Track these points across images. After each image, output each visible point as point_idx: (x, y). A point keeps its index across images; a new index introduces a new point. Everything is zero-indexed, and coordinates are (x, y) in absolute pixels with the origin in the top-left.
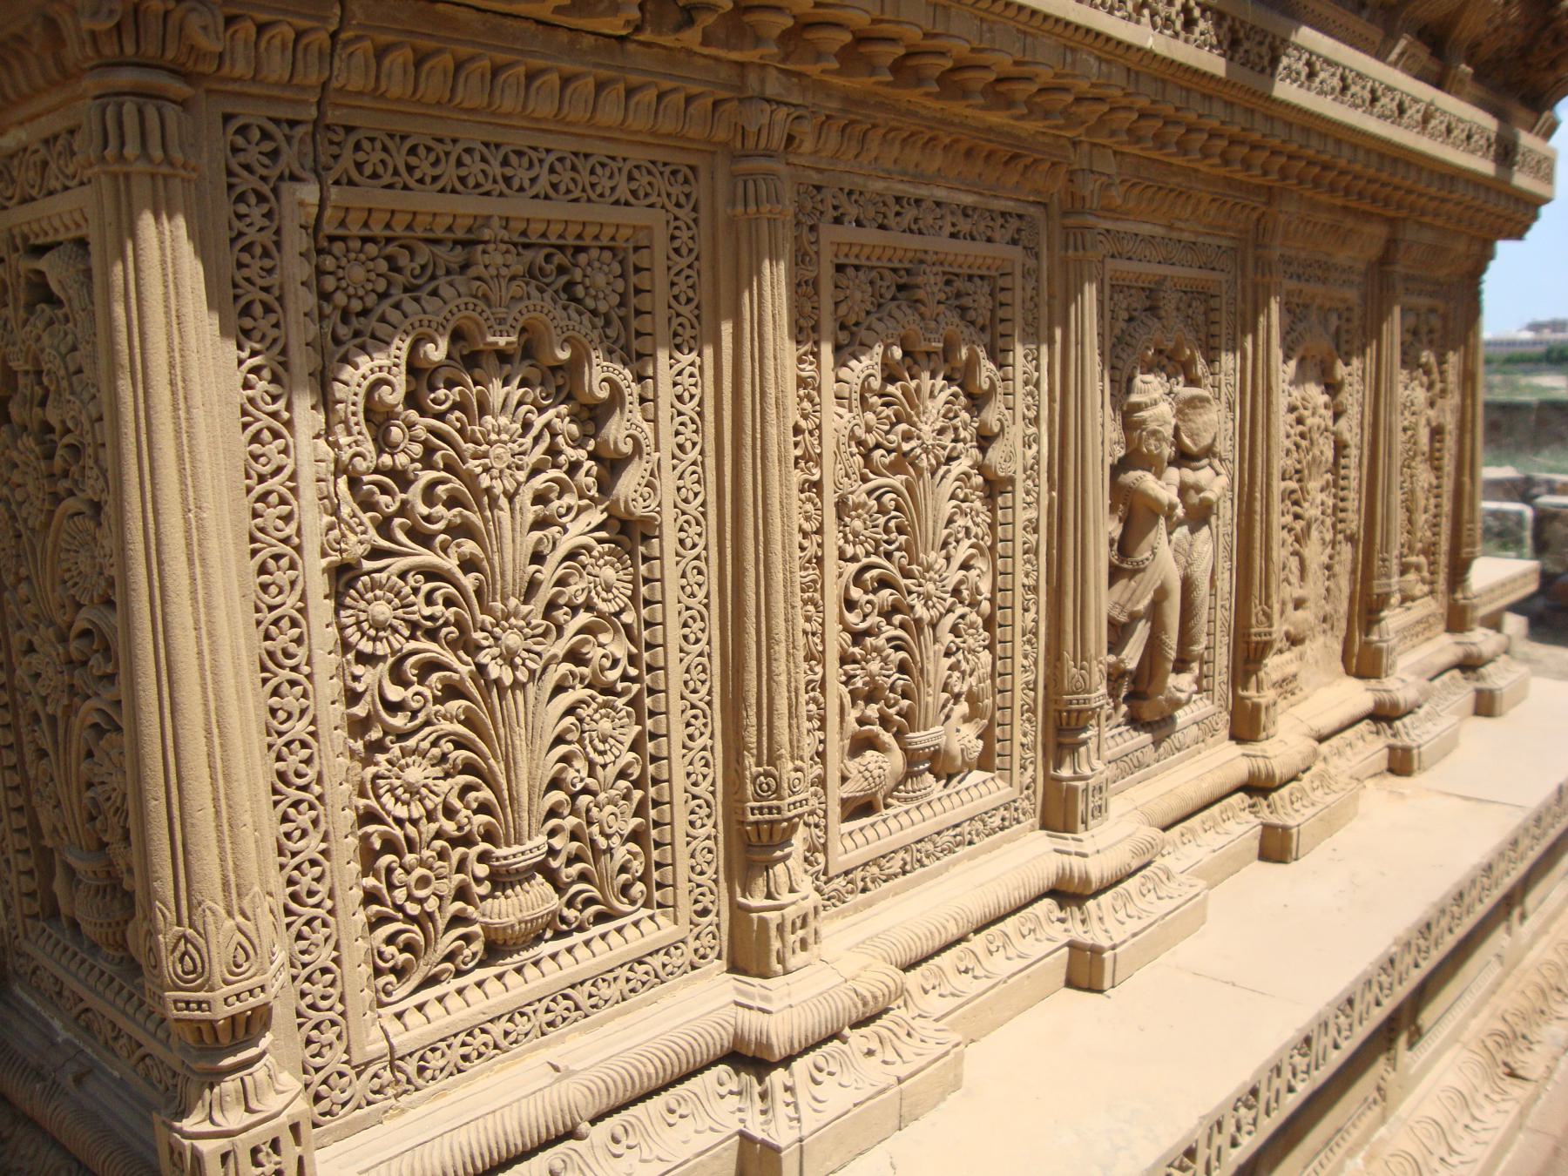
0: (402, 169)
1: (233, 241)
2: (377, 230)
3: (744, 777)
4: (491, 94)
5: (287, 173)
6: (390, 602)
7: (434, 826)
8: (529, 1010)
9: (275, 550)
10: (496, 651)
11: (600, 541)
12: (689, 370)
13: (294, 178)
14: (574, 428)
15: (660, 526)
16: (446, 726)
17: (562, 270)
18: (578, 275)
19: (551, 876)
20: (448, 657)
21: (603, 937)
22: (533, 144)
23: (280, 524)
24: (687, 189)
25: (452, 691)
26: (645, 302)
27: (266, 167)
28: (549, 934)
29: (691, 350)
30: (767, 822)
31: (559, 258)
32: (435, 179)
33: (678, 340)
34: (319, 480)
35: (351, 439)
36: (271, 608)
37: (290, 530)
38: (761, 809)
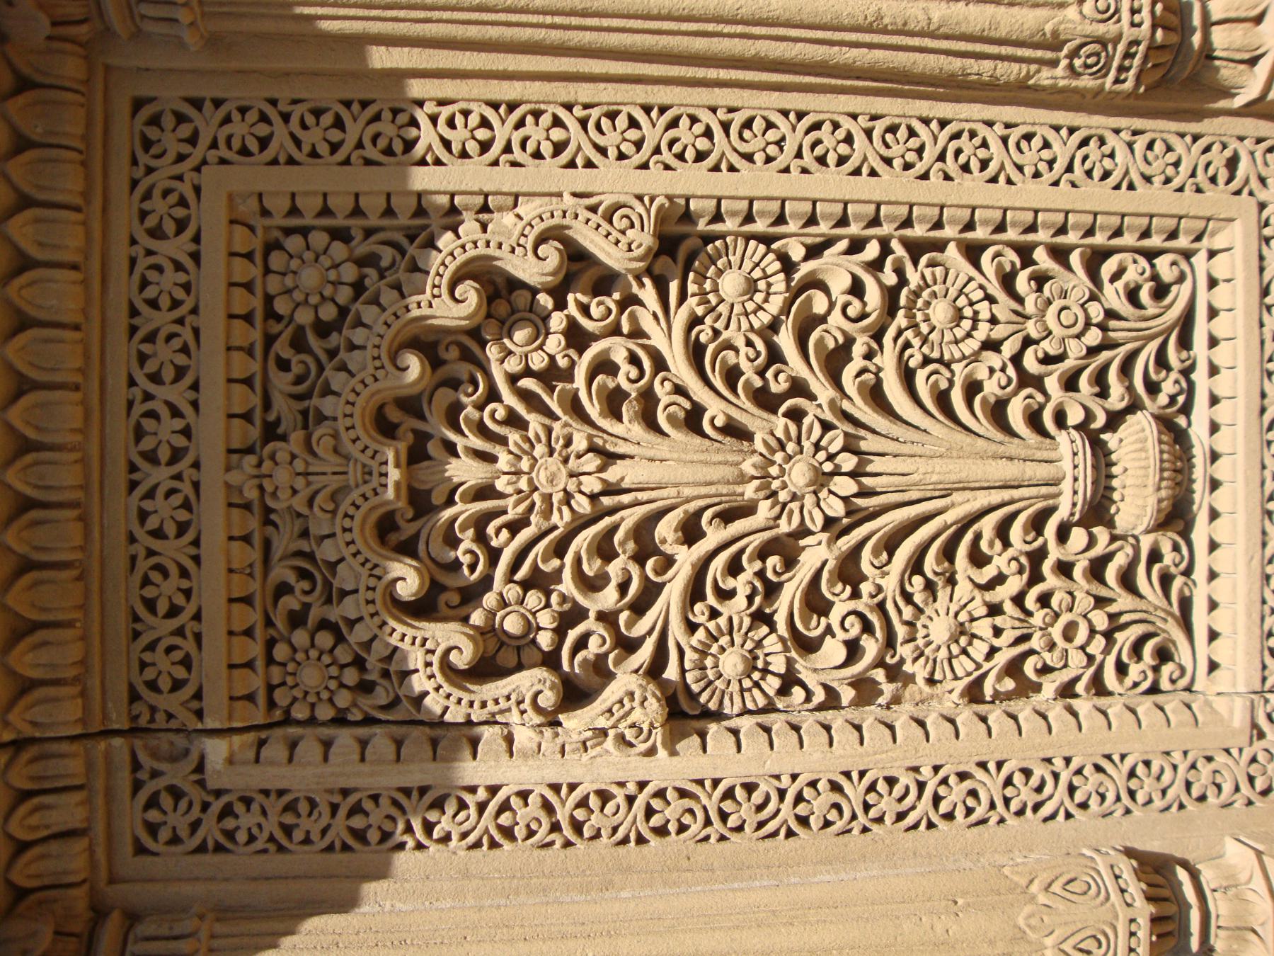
0: (174, 623)
1: (281, 849)
2: (255, 649)
4: (60, 505)
5: (196, 777)
6: (723, 649)
7: (1008, 607)
10: (809, 500)
11: (683, 297)
12: (442, 127)
13: (200, 768)
14: (520, 335)
15: (670, 198)
16: (890, 584)
17: (299, 343)
18: (304, 317)
20: (803, 572)
21: (1213, 342)
22: (124, 405)
23: (610, 807)
24: (168, 121)
25: (849, 572)
26: (342, 204)
27: (190, 804)
28: (1181, 421)
29: (414, 123)
31: (282, 348)
32: (184, 573)
33: (398, 146)
34: (563, 752)
35: (515, 711)
36: (708, 822)
38: (1122, 69)
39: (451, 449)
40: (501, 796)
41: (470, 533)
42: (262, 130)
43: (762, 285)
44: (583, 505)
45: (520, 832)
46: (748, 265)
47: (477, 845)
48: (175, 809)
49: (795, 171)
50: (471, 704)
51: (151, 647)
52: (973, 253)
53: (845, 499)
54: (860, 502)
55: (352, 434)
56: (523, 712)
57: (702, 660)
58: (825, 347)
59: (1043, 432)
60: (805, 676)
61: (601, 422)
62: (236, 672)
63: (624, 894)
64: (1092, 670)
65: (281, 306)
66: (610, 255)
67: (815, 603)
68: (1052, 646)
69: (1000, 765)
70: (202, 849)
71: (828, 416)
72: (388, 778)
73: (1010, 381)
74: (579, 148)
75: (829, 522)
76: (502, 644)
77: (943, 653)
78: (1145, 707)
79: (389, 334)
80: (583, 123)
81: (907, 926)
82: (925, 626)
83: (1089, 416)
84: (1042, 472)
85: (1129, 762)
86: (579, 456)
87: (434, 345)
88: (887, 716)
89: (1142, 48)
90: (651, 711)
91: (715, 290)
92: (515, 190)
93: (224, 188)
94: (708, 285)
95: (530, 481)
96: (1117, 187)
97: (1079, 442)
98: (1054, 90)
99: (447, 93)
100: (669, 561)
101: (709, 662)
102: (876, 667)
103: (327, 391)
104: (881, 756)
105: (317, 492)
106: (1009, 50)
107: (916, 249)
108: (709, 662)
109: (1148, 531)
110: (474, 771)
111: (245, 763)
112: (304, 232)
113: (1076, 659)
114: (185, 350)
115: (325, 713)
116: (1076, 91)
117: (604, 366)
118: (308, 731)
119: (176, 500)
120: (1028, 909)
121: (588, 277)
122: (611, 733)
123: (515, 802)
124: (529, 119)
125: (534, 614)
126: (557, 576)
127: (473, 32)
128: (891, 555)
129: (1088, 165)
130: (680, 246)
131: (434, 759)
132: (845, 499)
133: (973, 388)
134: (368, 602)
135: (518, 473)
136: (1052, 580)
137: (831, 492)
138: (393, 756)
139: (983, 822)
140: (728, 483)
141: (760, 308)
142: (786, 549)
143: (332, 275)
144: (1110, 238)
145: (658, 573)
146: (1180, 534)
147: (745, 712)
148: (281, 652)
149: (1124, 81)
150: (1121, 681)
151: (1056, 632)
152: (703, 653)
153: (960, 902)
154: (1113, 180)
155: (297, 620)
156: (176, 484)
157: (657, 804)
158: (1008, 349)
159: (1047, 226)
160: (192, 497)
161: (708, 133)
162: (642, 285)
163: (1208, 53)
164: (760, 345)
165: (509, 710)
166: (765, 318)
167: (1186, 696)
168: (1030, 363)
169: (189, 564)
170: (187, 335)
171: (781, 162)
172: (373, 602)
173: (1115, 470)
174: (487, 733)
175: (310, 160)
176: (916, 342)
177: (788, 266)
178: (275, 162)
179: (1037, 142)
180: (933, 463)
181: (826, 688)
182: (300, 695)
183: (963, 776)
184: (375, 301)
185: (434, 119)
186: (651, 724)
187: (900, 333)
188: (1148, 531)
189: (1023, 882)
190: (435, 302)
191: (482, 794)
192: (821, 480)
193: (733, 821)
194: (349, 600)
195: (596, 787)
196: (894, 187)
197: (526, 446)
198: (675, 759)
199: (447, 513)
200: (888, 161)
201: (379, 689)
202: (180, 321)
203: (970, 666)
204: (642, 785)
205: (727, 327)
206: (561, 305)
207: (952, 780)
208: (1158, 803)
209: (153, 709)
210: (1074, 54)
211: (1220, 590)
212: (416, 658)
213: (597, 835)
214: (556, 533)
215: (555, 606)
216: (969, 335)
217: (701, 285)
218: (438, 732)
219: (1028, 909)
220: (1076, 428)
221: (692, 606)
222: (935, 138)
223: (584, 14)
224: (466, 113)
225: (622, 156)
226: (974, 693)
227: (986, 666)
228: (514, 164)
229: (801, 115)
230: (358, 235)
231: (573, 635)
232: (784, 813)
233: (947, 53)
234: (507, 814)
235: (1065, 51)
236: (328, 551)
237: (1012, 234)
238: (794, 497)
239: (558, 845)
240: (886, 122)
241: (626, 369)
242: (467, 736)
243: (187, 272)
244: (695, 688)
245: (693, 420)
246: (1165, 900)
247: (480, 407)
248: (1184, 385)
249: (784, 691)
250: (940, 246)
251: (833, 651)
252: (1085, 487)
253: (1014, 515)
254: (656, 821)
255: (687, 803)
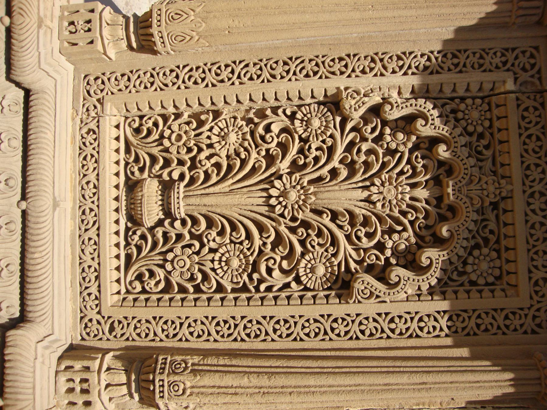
0: (528, 132)
1: (484, 50)
2: (497, 124)
3: (188, 355)
5: (517, 76)
6: (319, 128)
7: (205, 147)
8: (95, 198)
9: (349, 65)
10: (288, 186)
11: (339, 265)
13: (516, 79)
14: (403, 247)
16: (254, 155)
17: (486, 241)
18: (485, 251)
19: (160, 223)
21: (118, 257)
23: (361, 68)
25: (270, 159)
27: (519, 65)
28: (129, 225)
30: (154, 390)
31: (493, 238)
33: (455, 318)
35: (399, 103)
36: (323, 63)
37: (358, 72)
38: (165, 363)
39: (427, 202)
40: (403, 72)
41: (418, 170)
42: (508, 322)
43: (308, 271)
44: (377, 181)
45: (395, 58)
46: (314, 278)
47: (410, 53)
48: (524, 64)
49: (297, 316)
50: (416, 105)
51: (537, 123)
52: (220, 288)
53: (273, 187)
54: (267, 186)
55: (466, 205)
56: (396, 103)
57: (327, 124)
58: (282, 247)
59: (191, 217)
60: (286, 119)
61: (370, 214)
62: (504, 115)
63: (356, 35)
64: (168, 124)
65: (494, 254)
66: (368, 278)
67: (284, 147)
68: (186, 132)
69: (207, 86)
70: (513, 50)
71: (281, 219)
72: (445, 77)
73: (206, 237)
74: (384, 321)
75: (280, 177)
76: (403, 129)
77: (231, 129)
78: (146, 110)
79: (454, 244)
80: (383, 331)
81: (249, 23)
82: (238, 139)
83: (172, 225)
84: (192, 201)
85: (153, 88)
86: (379, 200)
87: (434, 242)
88: (252, 104)
89: (158, 371)
90: (348, 104)
91: (327, 268)
92: (409, 303)
93: (522, 299)
94: (330, 270)
95: (397, 190)
96: (161, 318)
97: (177, 213)
98: (192, 355)
99: (438, 340)
100: (341, 162)
101: (324, 124)
102: (257, 123)
103: (475, 222)
104: (256, 89)
105: (478, 183)
106: (213, 368)
107: (245, 289)
108: (324, 124)
109: (145, 179)
110: (414, 81)
111: (499, 82)
112: (487, 284)
113: (175, 127)
114: (532, 235)
115: (469, 101)
116: (183, 355)
117: (370, 236)
118: (475, 94)
119: (531, 178)
120: (201, 29)
121: (377, 271)
122: (362, 96)
123: (397, 69)
124: (404, 331)
125: (392, 140)
126: (384, 155)
127: (430, 363)
128: (254, 166)
129: (174, 326)
130: (342, 285)
131: (428, 85)
132: (273, 187)
133: (221, 233)
134: (457, 142)
135: (402, 193)
136: (186, 157)
137: (279, 190)
138: (444, 85)
139: (212, 64)
140: (321, 192)
141: (309, 262)
142: (295, 167)
143: (475, 267)
144: (162, 297)
145: (346, 156)
146: (130, 179)
147: (309, 105)
148: (487, 124)
149: (163, 359)
150: (156, 119)
151: (184, 138)
152: (327, 127)
153: (227, 32)
154: (163, 320)
155: (481, 136)
156: (531, 184)
157: (344, 69)
158: (206, 250)
159: (190, 301)
160: (525, 179)
161: (333, 330)
162: (355, 269)
163: (128, 372)
164: (309, 246)
165: (402, 103)
166: (307, 257)
167: (128, 115)
168: (197, 245)
169: (525, 154)
170: (531, 242)
171: (302, 320)
172: (455, 142)
173: (160, 203)
174: (408, 96)
175: (488, 311)
176: (245, 250)
177: (297, 280)
178: (502, 310)
179: (195, 334)
180: (237, 201)
181: (277, 115)
182: (479, 108)
183: (222, 81)
184: (459, 257)
185: (441, 330)
186: (347, 99)
187: (252, 254)
188: (145, 179)
189: (201, 40)
190: (437, 257)
191: (410, 72)
192: (284, 194)
193: (314, 63)
194: (463, 143)
195: (367, 75)
196: (255, 312)
197: (399, 203)
198: (337, 86)
199: (428, 177)
200: (258, 323)
201: (449, 110)
202: (534, 246)
203: (220, 124)
204: (349, 76)
205: (322, 253)
206: (387, 259)
207: (226, 80)
208: (141, 73)
209: (535, 100)
210: (186, 368)
211: (114, 157)
212: (437, 122)
213: (365, 57)
214: (386, 171)
215: (385, 143)
216: (223, 255)
217: (333, 270)
218: (426, 95)
219: (201, 29)
220: (177, 219)
221: (332, 145)
222: (239, 333)
223: (388, 372)
224: (429, 332)
225: (367, 319)
226: (217, 114)
227: (213, 124)
228: (409, 313)
229: (295, 339)
230: (466, 283)
231: (377, 133)
232: (292, 66)
233: (239, 366)
234: (400, 65)
235: (190, 369)
236: (472, 161)
237: (204, 297)
238: (294, 187)
239: (380, 53)
240: (260, 339)
241: (361, 234)
242: (415, 94)
243: (533, 266)
244: (329, 114)
245: (335, 216)
246: (142, 35)
247: (417, 218)
248: (129, 239)
249: (294, 114)
250: (234, 290)
251: (275, 128)
252: (174, 196)
253: (203, 183)
254: (343, 63)
255: (332, 70)
